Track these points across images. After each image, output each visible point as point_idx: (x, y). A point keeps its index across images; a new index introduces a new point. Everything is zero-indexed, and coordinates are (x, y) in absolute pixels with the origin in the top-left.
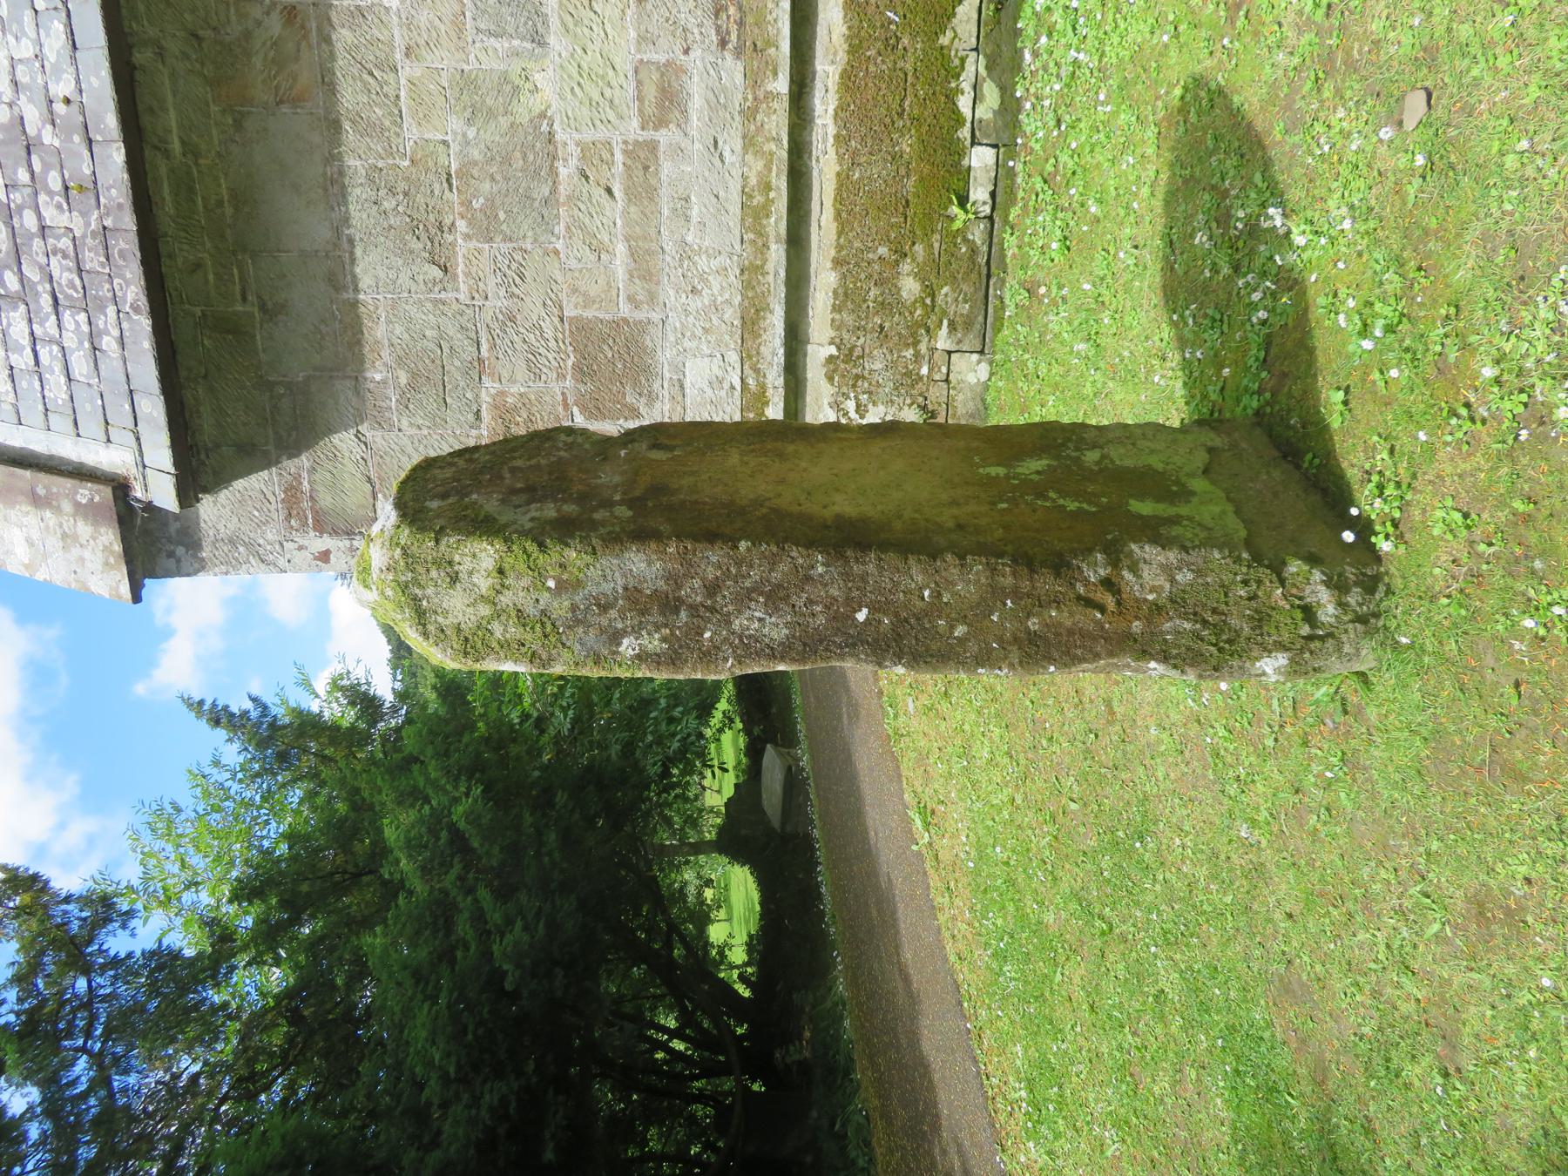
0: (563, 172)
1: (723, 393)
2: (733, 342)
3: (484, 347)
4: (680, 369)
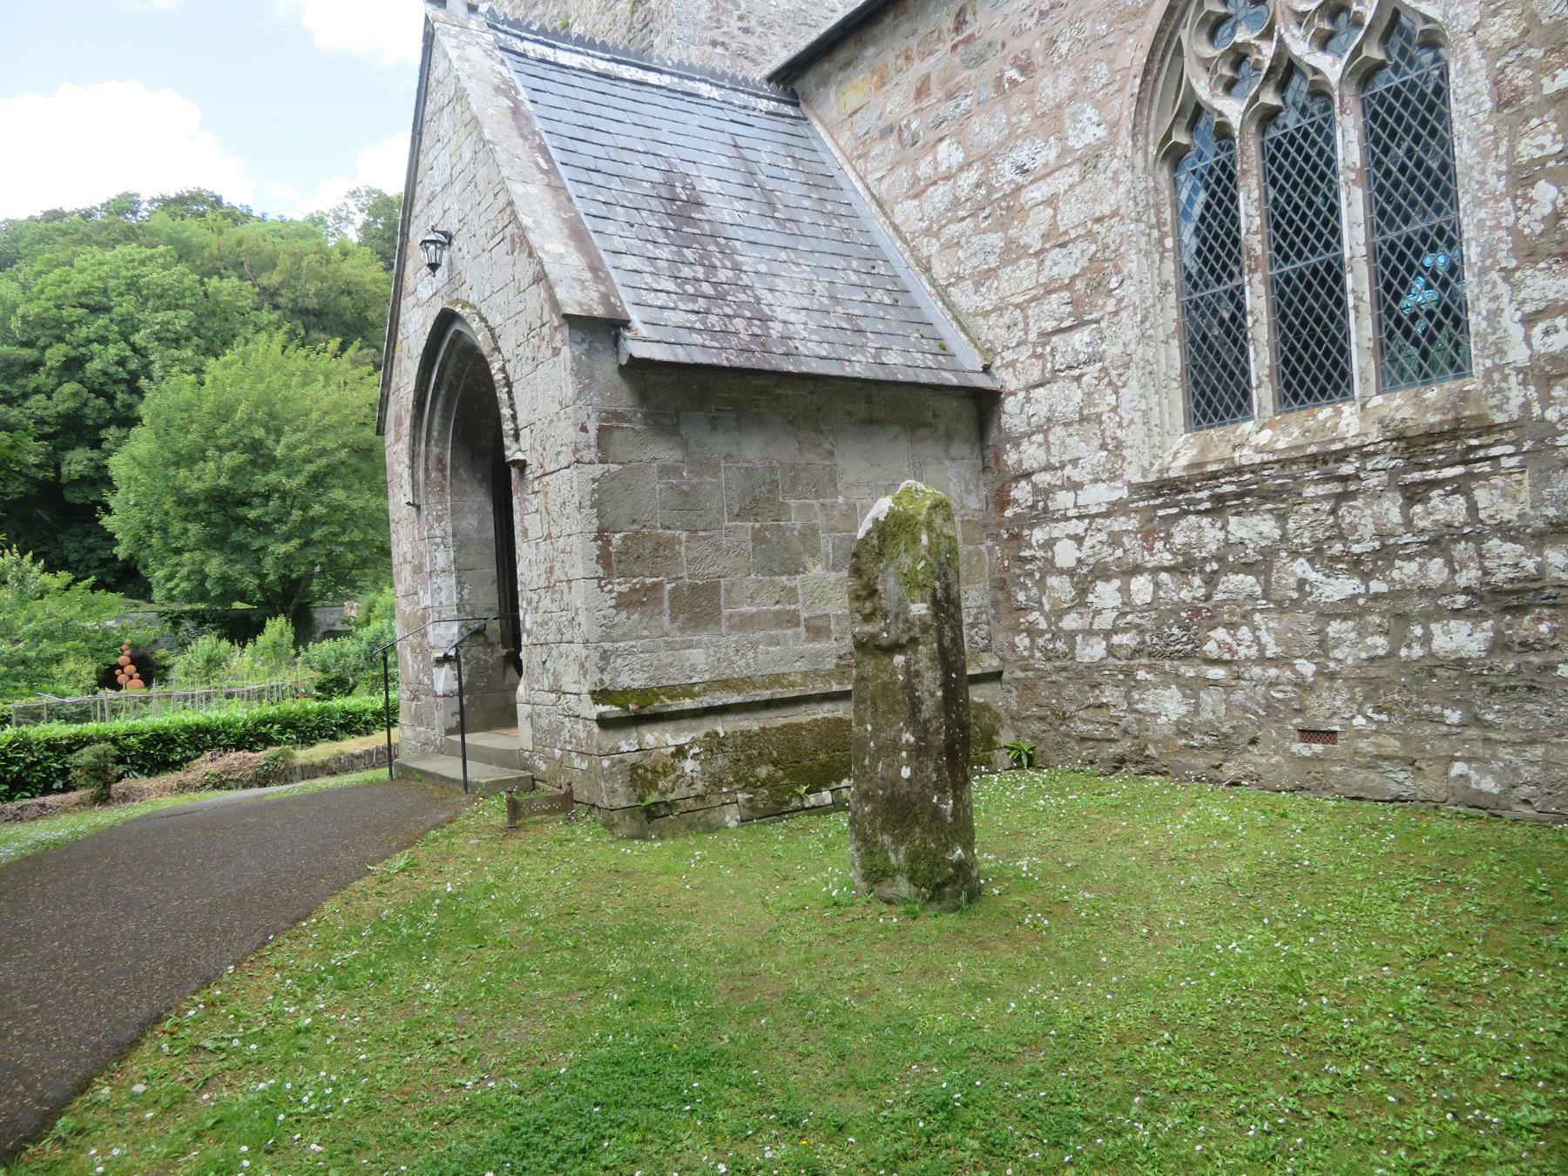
0: (784, 578)
4: (699, 645)
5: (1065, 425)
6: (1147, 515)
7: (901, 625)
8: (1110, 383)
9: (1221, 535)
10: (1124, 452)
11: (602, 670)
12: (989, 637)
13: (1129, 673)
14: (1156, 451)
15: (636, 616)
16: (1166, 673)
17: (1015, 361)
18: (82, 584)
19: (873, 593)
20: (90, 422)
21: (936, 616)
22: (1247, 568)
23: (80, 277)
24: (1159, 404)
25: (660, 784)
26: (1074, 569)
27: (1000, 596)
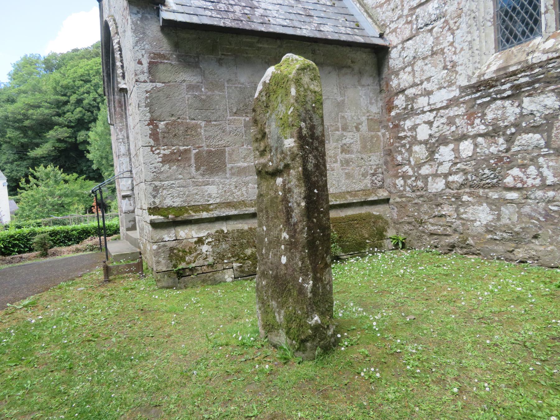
1: (206, 198)
2: (223, 200)
3: (215, 123)
4: (213, 183)
5: (423, 59)
6: (470, 104)
7: (279, 156)
8: (449, 29)
9: (518, 110)
10: (457, 69)
11: (154, 197)
12: (383, 181)
13: (458, 197)
14: (477, 65)
15: (175, 167)
16: (480, 197)
17: (397, 28)
18: (81, 178)
19: (264, 135)
20: (86, 121)
21: (301, 147)
22: (535, 129)
23: (81, 70)
24: (479, 36)
25: (187, 258)
26: (428, 140)
27: (389, 159)
